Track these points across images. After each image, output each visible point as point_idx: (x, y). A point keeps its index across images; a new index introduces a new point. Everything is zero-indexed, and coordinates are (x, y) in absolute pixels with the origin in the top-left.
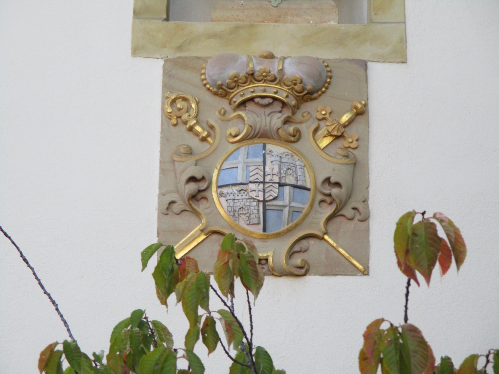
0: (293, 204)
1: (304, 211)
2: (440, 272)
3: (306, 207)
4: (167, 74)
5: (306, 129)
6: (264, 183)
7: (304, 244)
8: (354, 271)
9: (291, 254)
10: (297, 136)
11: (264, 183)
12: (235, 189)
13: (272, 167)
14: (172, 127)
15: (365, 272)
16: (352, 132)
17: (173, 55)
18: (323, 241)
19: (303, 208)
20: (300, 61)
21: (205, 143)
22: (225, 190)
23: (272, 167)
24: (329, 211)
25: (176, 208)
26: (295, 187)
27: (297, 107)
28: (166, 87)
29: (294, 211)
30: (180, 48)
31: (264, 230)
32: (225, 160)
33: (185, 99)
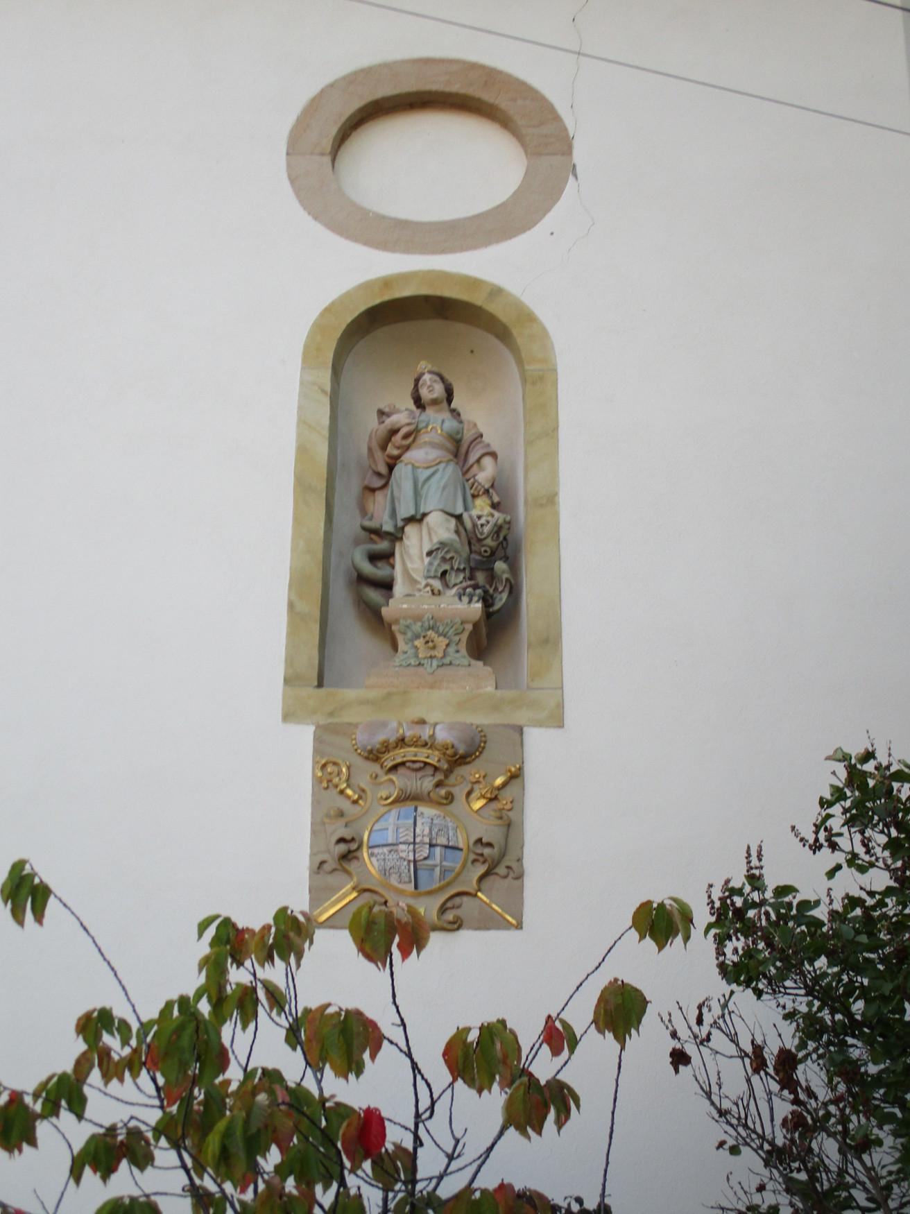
0: (444, 863)
1: (457, 870)
2: (303, 451)
3: (458, 866)
4: (318, 740)
5: (460, 792)
6: (414, 843)
7: (457, 900)
8: (508, 926)
9: (443, 910)
10: (450, 798)
11: (414, 843)
12: (386, 850)
13: (423, 829)
14: (323, 792)
15: (519, 926)
16: (507, 795)
17: (323, 720)
18: (476, 899)
19: (455, 868)
20: (451, 727)
21: (356, 806)
22: (376, 851)
23: (423, 829)
24: (481, 869)
25: (327, 867)
26: (447, 847)
27: (448, 773)
28: (317, 751)
29: (444, 871)
30: (331, 714)
31: (416, 887)
32: (377, 821)
33: (335, 764)
